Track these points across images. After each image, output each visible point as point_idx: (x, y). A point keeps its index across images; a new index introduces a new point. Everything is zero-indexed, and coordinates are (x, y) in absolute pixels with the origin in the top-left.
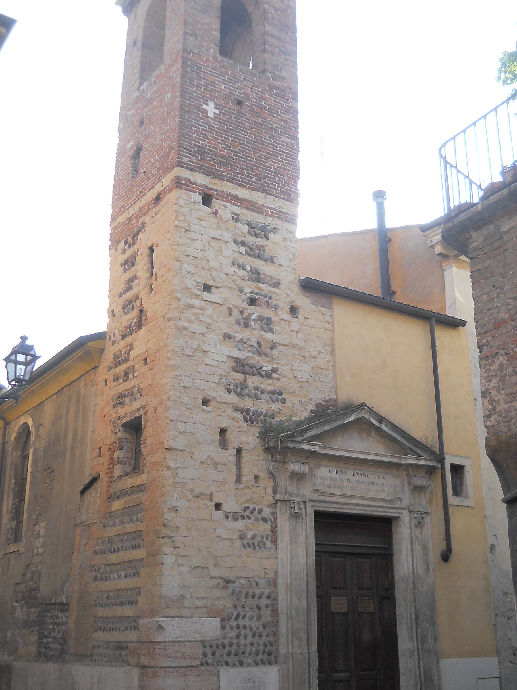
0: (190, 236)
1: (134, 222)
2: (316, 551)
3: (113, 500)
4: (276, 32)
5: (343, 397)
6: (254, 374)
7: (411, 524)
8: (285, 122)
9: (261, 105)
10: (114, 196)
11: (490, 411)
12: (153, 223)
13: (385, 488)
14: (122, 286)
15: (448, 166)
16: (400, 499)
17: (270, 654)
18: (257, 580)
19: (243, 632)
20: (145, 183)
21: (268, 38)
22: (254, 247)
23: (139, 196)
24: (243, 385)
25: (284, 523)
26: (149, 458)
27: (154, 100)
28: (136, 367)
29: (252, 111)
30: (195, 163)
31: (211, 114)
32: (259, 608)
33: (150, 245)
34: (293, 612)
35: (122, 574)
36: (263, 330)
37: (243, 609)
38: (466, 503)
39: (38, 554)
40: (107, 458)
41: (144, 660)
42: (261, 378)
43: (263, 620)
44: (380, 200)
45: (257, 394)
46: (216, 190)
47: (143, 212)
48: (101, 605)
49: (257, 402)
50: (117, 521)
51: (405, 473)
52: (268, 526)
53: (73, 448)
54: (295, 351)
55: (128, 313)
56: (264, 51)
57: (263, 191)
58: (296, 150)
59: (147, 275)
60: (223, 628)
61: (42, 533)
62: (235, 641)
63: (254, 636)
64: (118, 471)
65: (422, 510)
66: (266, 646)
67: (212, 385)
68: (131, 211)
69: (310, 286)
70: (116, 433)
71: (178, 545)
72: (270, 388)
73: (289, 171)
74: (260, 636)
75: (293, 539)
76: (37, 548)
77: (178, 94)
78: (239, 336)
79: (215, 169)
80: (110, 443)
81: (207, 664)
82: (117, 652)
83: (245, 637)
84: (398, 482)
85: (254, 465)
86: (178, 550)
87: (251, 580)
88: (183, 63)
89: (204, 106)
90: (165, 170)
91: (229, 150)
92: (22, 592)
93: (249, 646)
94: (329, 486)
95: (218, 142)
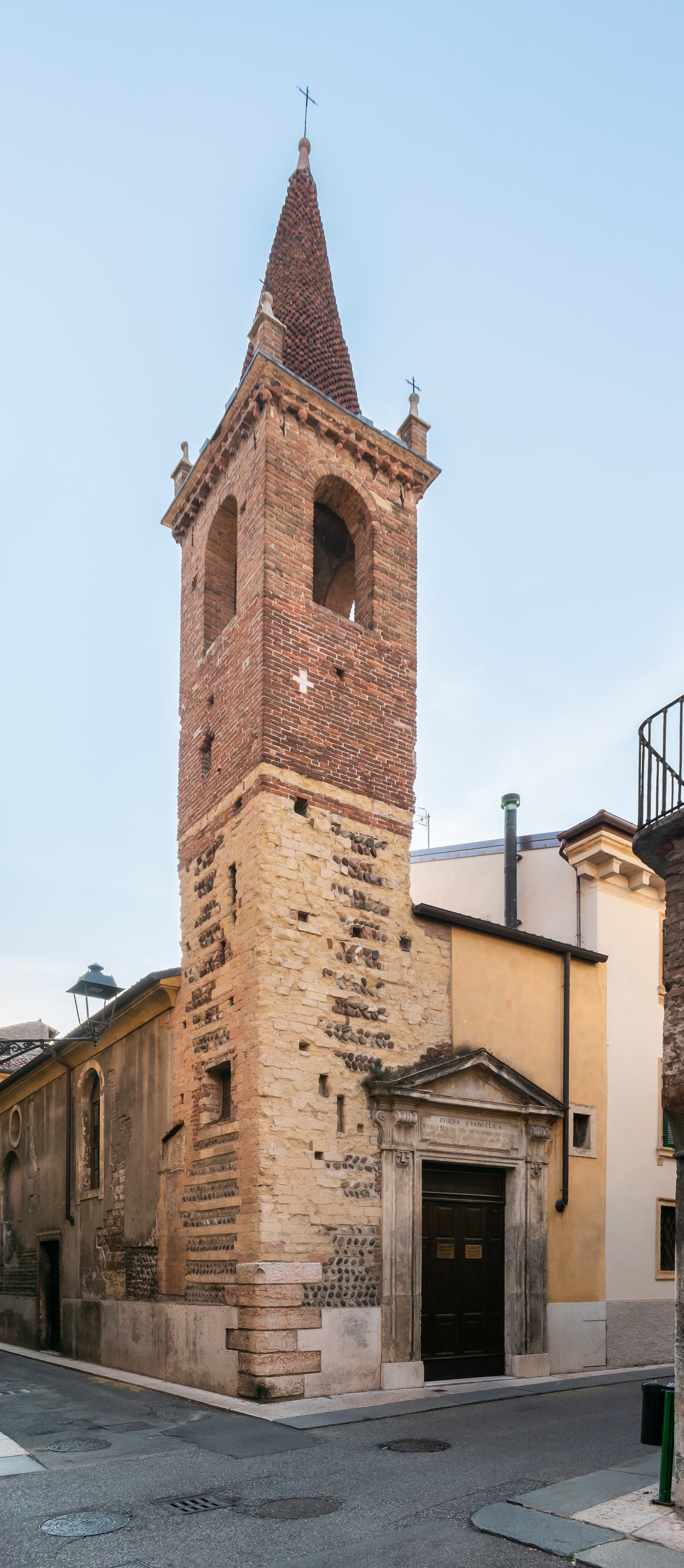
0: (281, 852)
1: (208, 835)
2: (423, 1200)
3: (202, 1148)
4: (389, 565)
5: (459, 1041)
6: (357, 1016)
7: (527, 1175)
8: (399, 699)
9: (368, 675)
10: (180, 803)
11: (672, 1058)
12: (234, 836)
13: (501, 1139)
14: (198, 914)
15: (654, 758)
16: (516, 1150)
17: (372, 1296)
19: (345, 1276)
20: (221, 785)
21: (377, 574)
22: (359, 867)
23: (213, 802)
24: (346, 1028)
25: (389, 1171)
26: (240, 1106)
27: (227, 669)
28: (220, 1008)
29: (357, 684)
30: (285, 757)
31: (303, 689)
32: (362, 1254)
33: (230, 864)
34: (398, 1258)
35: (216, 1220)
36: (368, 965)
38: (588, 1154)
39: (119, 1201)
40: (191, 1105)
41: (243, 1301)
42: (365, 1021)
43: (366, 1265)
44: (511, 807)
45: (361, 1038)
46: (312, 794)
47: (220, 823)
48: (193, 1250)
49: (360, 1047)
50: (207, 1169)
52: (372, 1176)
53: (150, 1095)
54: (404, 990)
55: (207, 946)
56: (372, 595)
57: (370, 795)
58: (412, 739)
59: (229, 900)
60: (325, 1271)
61: (122, 1180)
62: (337, 1284)
63: (356, 1279)
64: (205, 1118)
65: (540, 1161)
67: (311, 1028)
68: (204, 822)
69: (425, 915)
70: (200, 1079)
71: (276, 1193)
72: (375, 1031)
73: (402, 767)
74: (363, 1279)
75: (399, 1188)
76: (118, 1195)
77: (259, 659)
78: (340, 973)
79: (310, 765)
80: (193, 1089)
81: (309, 1304)
82: (214, 1293)
83: (348, 1281)
84: (515, 1132)
85: (358, 1113)
86: (276, 1198)
87: (354, 1227)
88: (265, 613)
89: (295, 678)
90: (245, 766)
91: (328, 739)
92: (105, 1236)
93: (351, 1288)
94: (439, 1136)
95: (314, 729)
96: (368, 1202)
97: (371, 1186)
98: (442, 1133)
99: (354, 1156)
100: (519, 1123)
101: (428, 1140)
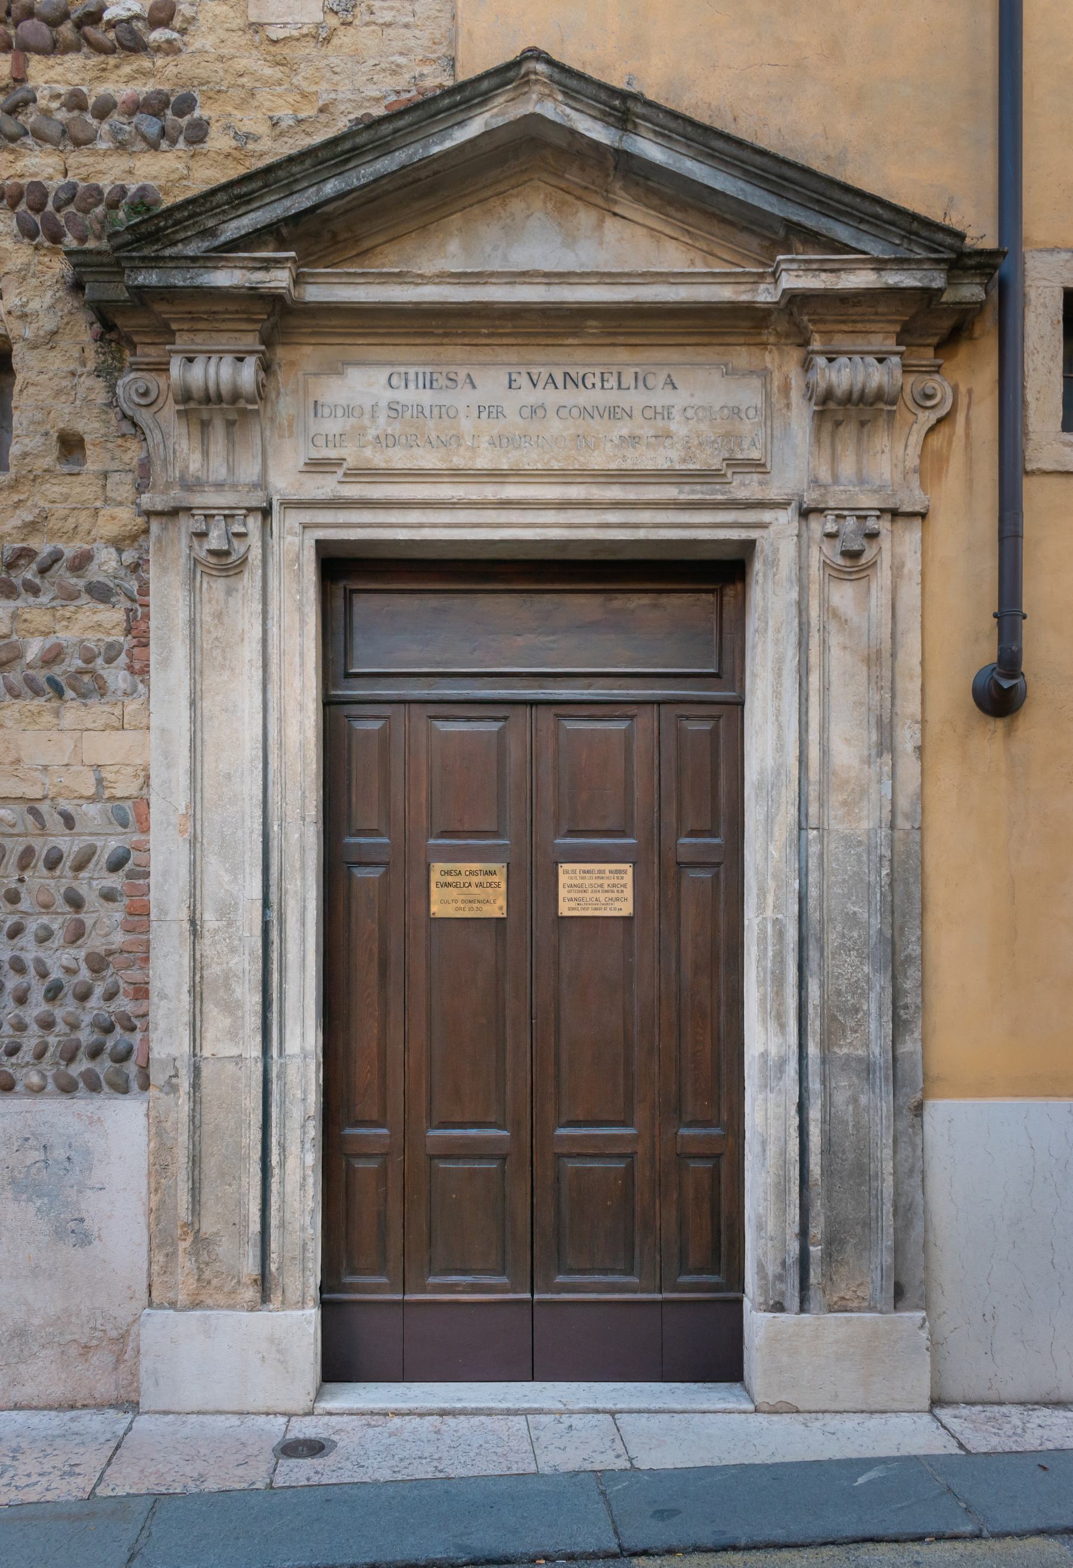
7: (802, 567)
13: (678, 427)
16: (758, 466)
17: (123, 1057)
18: (65, 805)
32: (75, 902)
37: (10, 907)
42: (96, 60)
43: (95, 943)
51: (795, 355)
52: (112, 616)
63: (54, 993)
65: (867, 501)
66: (108, 1029)
72: (144, 88)
83: (21, 999)
84: (748, 395)
87: (44, 807)
93: (34, 1028)
96: (98, 711)
97: (111, 654)
98: (396, 428)
99: (43, 547)
100: (769, 359)
101: (339, 462)
